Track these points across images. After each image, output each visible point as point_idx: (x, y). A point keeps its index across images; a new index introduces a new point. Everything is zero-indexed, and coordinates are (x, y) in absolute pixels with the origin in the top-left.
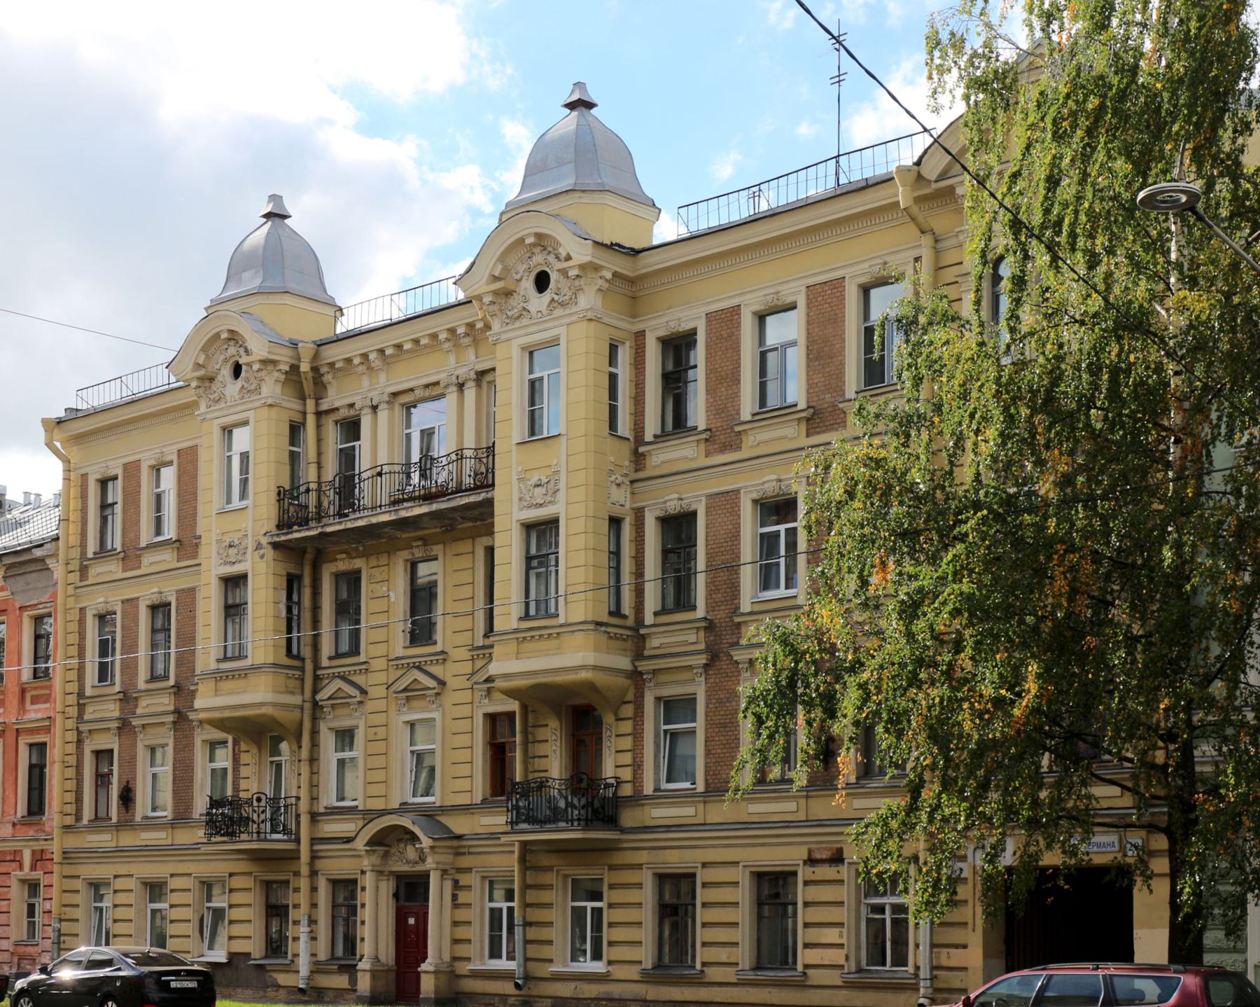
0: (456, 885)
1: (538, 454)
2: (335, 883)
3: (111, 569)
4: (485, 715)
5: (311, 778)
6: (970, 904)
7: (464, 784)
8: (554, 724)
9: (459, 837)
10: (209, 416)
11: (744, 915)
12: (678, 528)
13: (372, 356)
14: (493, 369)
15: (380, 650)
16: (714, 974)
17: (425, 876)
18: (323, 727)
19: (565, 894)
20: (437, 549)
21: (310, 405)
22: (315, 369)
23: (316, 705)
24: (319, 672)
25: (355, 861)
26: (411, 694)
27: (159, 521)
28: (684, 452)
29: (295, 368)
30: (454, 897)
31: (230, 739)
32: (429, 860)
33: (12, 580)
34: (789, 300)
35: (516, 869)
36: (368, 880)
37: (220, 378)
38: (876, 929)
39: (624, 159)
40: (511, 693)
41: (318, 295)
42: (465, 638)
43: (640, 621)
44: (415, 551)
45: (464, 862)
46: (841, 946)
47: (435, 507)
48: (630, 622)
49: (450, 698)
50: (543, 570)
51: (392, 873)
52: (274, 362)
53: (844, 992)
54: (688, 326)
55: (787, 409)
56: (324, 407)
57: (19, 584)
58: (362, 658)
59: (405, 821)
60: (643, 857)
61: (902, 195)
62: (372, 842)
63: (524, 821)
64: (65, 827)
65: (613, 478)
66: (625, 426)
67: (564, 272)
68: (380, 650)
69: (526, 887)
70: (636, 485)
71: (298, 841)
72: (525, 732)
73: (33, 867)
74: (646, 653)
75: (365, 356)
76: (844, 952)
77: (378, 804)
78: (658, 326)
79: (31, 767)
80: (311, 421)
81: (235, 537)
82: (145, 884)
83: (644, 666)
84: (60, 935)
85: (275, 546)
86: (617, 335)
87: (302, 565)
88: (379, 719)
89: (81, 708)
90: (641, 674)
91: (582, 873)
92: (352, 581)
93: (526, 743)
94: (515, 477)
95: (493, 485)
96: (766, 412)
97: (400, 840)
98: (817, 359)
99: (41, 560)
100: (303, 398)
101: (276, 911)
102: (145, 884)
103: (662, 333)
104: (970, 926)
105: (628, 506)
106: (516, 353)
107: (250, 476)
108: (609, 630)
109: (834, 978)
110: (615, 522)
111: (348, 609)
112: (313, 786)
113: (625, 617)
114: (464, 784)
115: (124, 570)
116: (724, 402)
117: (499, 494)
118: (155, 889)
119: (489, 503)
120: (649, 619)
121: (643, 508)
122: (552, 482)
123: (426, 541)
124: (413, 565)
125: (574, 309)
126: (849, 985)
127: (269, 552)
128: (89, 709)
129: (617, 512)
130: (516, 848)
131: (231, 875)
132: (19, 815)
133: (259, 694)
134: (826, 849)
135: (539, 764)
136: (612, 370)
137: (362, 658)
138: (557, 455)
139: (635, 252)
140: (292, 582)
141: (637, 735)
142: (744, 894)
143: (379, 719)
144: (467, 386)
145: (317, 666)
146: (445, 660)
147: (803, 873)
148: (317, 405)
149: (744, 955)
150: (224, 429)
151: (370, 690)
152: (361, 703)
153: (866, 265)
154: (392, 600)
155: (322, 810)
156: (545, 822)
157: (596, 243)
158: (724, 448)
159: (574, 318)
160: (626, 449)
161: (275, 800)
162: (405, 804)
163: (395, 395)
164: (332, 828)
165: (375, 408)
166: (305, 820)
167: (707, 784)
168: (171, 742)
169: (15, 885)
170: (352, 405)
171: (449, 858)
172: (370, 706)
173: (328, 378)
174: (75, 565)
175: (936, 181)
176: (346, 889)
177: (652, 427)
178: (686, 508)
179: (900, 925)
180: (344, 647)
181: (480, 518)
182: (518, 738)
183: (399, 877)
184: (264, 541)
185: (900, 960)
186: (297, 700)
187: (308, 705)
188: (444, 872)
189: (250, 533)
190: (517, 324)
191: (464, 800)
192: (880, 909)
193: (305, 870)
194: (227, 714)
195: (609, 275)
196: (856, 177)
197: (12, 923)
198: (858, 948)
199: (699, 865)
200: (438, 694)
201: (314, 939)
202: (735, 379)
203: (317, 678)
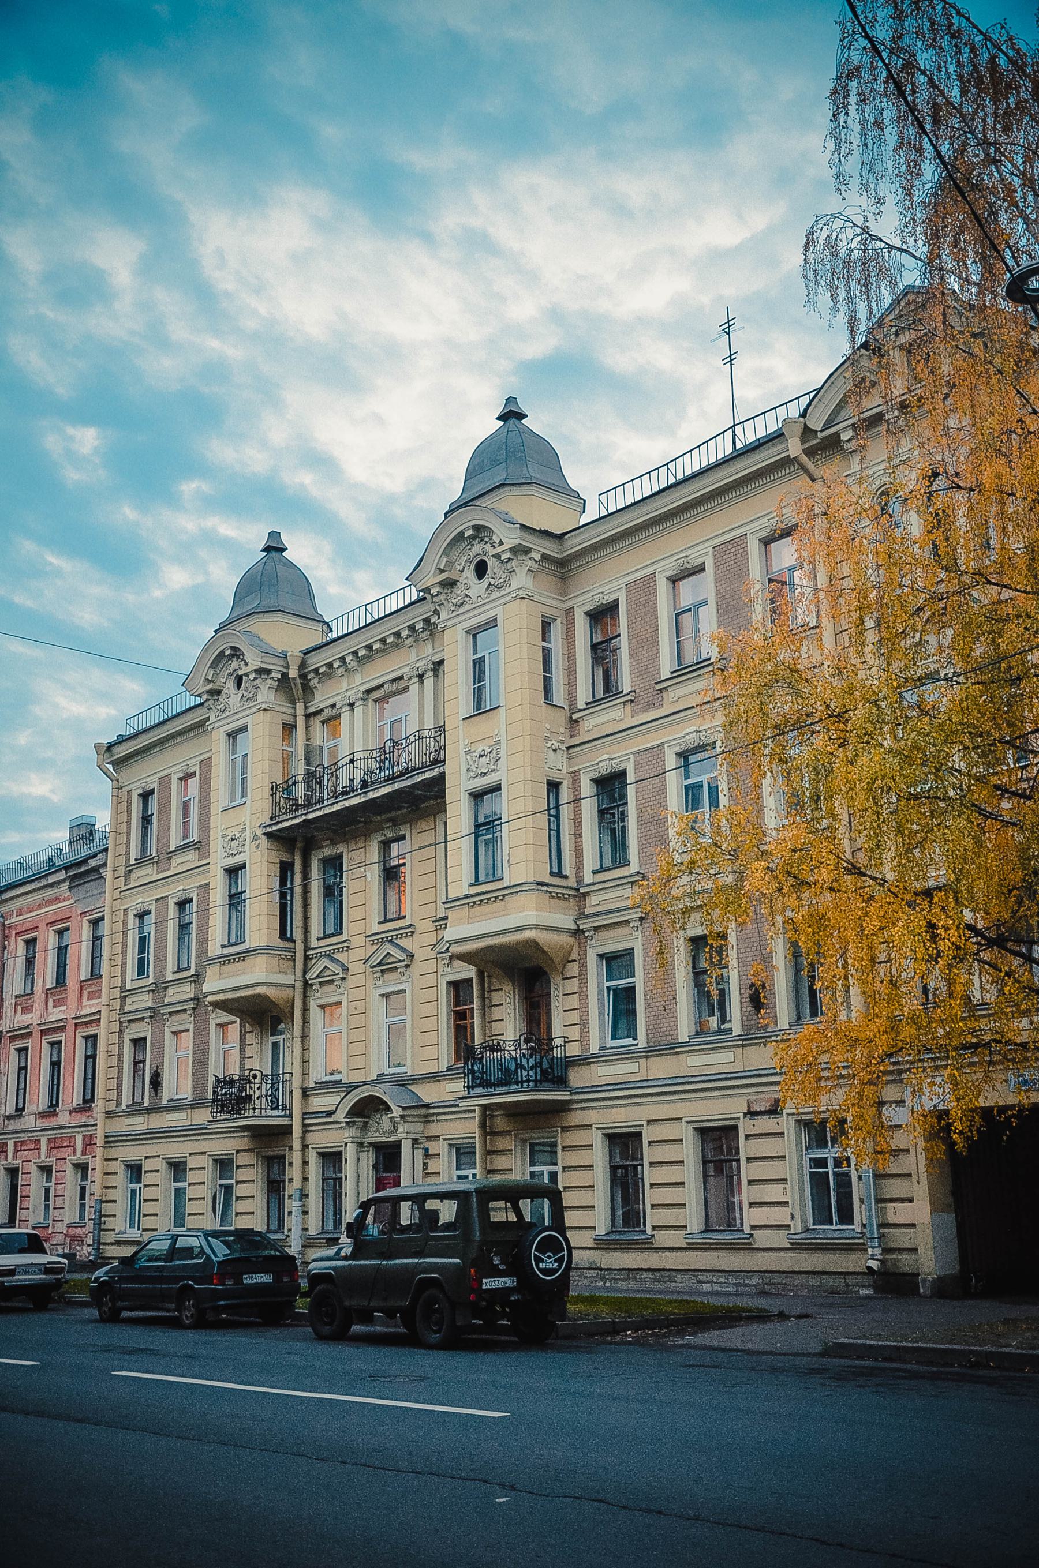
0: (427, 1155)
1: (483, 726)
2: (324, 1156)
3: (149, 873)
4: (449, 983)
5: (303, 1055)
6: (912, 1152)
7: (431, 1052)
8: (508, 987)
9: (427, 1106)
10: (216, 725)
11: (691, 1173)
12: (611, 785)
13: (348, 659)
14: (498, 788)
15: (359, 927)
16: (663, 1238)
17: (397, 1145)
18: (312, 1005)
19: (523, 1161)
20: (405, 830)
21: (300, 706)
22: (303, 676)
23: (306, 985)
24: (309, 953)
25: (335, 1136)
26: (385, 967)
27: (186, 825)
28: (613, 716)
29: (285, 675)
30: (425, 1165)
31: (238, 1020)
32: (401, 1129)
33: (76, 889)
34: (699, 561)
35: (477, 1135)
36: (350, 1153)
37: (225, 691)
38: (819, 1182)
39: (550, 459)
40: (466, 957)
41: (307, 611)
42: (429, 911)
43: (580, 881)
44: (386, 832)
45: (433, 1129)
46: (785, 1204)
47: (396, 786)
48: (572, 882)
49: (417, 968)
50: (490, 836)
51: (371, 1144)
52: (268, 672)
53: (791, 1254)
54: (611, 598)
55: (702, 664)
56: (312, 710)
57: (81, 892)
58: (344, 937)
59: (377, 1092)
60: (592, 1116)
61: (794, 448)
62: (351, 1113)
63: (479, 1086)
64: (107, 1112)
65: (550, 743)
66: (559, 696)
67: (497, 556)
68: (359, 927)
69: (488, 1152)
70: (571, 751)
71: (291, 1116)
72: (482, 997)
73: (84, 1153)
74: (587, 911)
75: (342, 659)
76: (789, 1210)
77: (357, 1077)
78: (584, 601)
79: (87, 1057)
80: (300, 722)
81: (235, 832)
82: (215, 1161)
83: (586, 924)
84: (101, 1216)
85: (269, 835)
86: (550, 612)
87: (293, 854)
88: (359, 993)
89: (123, 999)
90: (583, 932)
91: (537, 1136)
92: (334, 865)
93: (483, 1007)
94: (462, 751)
95: (444, 761)
96: (685, 671)
97: (377, 1111)
98: (726, 612)
99: (95, 870)
100: (293, 702)
101: (275, 1188)
102: (170, 1164)
103: (588, 608)
104: (914, 1178)
105: (564, 771)
106: (461, 635)
107: (249, 775)
108: (550, 889)
109: (780, 1239)
110: (553, 786)
111: (332, 893)
112: (305, 1062)
113: (566, 877)
114: (431, 1052)
115: (158, 873)
116: (645, 668)
117: (448, 768)
118: (178, 1168)
119: (442, 776)
120: (588, 878)
121: (578, 771)
122: (494, 752)
123: (395, 823)
124: (386, 845)
125: (508, 590)
126: (796, 1247)
127: (264, 841)
128: (129, 1001)
129: (555, 776)
130: (477, 1114)
131: (238, 1152)
132: (75, 1104)
133: (259, 975)
134: (764, 1100)
135: (496, 1028)
136: (546, 644)
137: (344, 937)
138: (497, 725)
139: (561, 537)
140: (285, 869)
141: (583, 994)
142: (690, 1151)
143: (359, 993)
144: (426, 676)
145: (307, 948)
146: (413, 932)
147: (744, 1127)
148: (306, 708)
149: (693, 1219)
150: (229, 735)
151: (350, 966)
152: (343, 979)
153: (765, 520)
154: (369, 880)
155: (312, 1085)
156: (498, 1085)
157: (524, 527)
158: (650, 705)
159: (509, 598)
160: (561, 717)
161: (275, 1075)
162: (382, 1075)
163: (369, 692)
164: (318, 1102)
165: (352, 705)
166: (297, 1094)
167: (648, 1040)
168: (191, 1027)
169: (69, 1168)
170: (333, 706)
171: (419, 1127)
172: (352, 981)
173: (314, 682)
174: (122, 871)
175: (821, 431)
176: (332, 1159)
177: (583, 696)
178: (616, 768)
179: (844, 1182)
180: (330, 930)
181: (436, 788)
182: (476, 1004)
183: (378, 1147)
184: (259, 832)
185: (846, 1216)
186: (289, 979)
187: (299, 985)
188: (415, 1141)
189: (247, 826)
190: (461, 611)
191: (431, 1068)
192: (821, 1163)
193: (297, 1145)
194: (229, 996)
195: (538, 557)
196: (751, 439)
197: (66, 1206)
198: (804, 1206)
199: (645, 1123)
200: (407, 966)
201: (306, 1213)
202: (655, 641)
203: (307, 958)
